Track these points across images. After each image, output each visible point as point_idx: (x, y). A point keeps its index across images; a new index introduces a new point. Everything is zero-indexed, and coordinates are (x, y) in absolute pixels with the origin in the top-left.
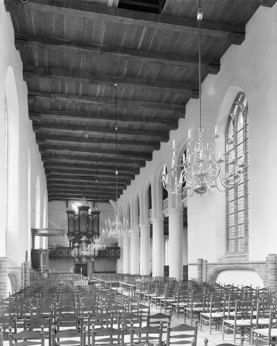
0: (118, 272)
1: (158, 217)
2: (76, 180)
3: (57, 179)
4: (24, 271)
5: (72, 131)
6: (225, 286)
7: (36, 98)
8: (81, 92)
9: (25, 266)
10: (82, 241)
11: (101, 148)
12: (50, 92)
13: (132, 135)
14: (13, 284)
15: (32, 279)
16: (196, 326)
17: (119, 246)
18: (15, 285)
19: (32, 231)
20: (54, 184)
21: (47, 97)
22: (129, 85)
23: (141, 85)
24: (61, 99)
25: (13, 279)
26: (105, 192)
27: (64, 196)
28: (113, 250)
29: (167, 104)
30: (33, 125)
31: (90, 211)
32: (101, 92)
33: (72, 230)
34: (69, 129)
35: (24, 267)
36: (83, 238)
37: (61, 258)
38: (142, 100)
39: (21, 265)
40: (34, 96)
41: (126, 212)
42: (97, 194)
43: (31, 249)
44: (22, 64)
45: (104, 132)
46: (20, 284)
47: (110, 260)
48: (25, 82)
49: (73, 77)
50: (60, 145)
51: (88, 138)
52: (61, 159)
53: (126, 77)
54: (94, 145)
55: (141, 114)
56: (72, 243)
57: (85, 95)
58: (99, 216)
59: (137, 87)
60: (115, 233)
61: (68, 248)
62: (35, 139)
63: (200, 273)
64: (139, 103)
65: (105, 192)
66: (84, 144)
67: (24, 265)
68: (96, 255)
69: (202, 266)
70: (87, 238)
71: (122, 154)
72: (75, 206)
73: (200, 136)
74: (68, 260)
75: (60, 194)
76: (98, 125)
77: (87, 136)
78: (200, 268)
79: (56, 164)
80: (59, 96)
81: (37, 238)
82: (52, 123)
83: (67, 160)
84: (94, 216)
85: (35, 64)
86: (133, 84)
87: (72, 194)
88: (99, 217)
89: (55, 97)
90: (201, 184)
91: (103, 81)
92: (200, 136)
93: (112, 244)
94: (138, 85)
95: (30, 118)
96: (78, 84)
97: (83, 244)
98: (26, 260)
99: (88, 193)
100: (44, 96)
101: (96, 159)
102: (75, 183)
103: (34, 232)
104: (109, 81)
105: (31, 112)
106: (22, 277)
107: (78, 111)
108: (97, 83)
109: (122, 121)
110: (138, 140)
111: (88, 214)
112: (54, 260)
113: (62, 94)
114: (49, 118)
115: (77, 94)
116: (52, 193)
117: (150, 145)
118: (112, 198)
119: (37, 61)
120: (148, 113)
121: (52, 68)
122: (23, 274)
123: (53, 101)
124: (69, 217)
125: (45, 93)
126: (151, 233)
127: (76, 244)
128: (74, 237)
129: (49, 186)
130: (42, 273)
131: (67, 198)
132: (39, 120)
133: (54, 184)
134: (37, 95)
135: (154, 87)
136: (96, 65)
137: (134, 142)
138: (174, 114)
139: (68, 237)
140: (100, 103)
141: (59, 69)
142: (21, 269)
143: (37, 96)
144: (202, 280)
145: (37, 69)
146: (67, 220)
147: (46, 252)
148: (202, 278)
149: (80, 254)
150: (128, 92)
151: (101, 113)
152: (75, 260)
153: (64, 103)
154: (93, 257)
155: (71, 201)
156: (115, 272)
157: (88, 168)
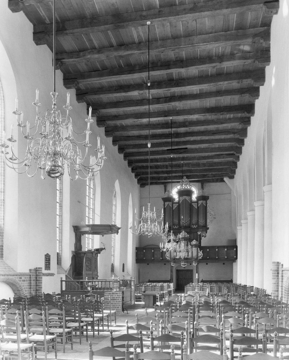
3: (138, 158)
5: (124, 93)
21: (76, 58)
22: (167, 18)
24: (92, 57)
26: (211, 168)
28: (226, 250)
29: (240, 31)
32: (139, 36)
34: (121, 92)
37: (153, 261)
39: (28, 271)
45: (166, 88)
47: (224, 264)
49: (92, 26)
50: (121, 113)
51: (153, 99)
53: (161, 9)
55: (209, 53)
57: (122, 45)
59: (178, 18)
60: (147, 228)
65: (211, 168)
68: (200, 258)
70: (186, 233)
73: (54, 102)
76: (156, 79)
80: (89, 53)
82: (99, 88)
84: (200, 202)
85: (46, 21)
86: (171, 16)
88: (206, 204)
91: (130, 21)
92: (54, 102)
93: (229, 241)
94: (178, 15)
100: (72, 58)
102: (165, 160)
107: (123, 67)
108: (123, 27)
109: (183, 68)
113: (93, 50)
114: (89, 82)
116: (142, 176)
117: (243, 93)
118: (226, 175)
119: (47, 18)
121: (66, 22)
125: (72, 54)
134: (63, 58)
135: (203, 13)
137: (219, 93)
140: (141, 51)
143: (64, 59)
147: (91, 254)
150: (175, 27)
156: (232, 281)
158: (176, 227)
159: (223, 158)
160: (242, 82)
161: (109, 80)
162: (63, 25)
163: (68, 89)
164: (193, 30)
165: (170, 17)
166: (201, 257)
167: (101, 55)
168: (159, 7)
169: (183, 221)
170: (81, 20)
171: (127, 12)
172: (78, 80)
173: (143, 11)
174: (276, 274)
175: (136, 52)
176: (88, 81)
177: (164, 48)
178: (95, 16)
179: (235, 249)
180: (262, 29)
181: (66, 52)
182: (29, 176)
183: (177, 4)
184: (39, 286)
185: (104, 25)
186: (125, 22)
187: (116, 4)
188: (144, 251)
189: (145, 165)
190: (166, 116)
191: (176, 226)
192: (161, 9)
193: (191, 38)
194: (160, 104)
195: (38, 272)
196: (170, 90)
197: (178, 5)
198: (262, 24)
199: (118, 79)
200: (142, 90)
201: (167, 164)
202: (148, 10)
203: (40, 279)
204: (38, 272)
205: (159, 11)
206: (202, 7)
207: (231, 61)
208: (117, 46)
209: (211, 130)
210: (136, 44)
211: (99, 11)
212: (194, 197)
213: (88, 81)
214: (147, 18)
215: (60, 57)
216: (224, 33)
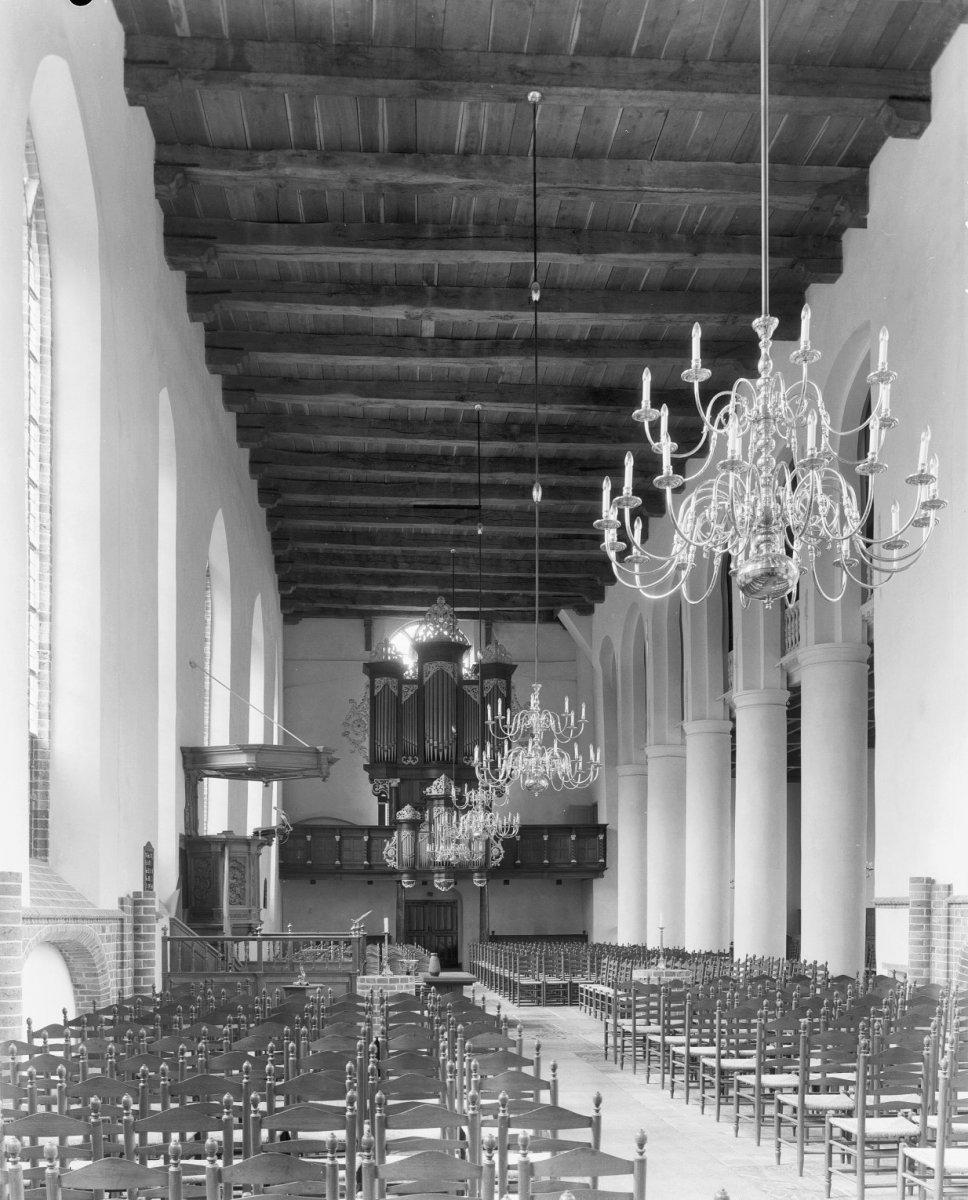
0: (597, 938)
1: (762, 687)
2: (403, 527)
4: (128, 932)
6: (32, 1035)
7: (190, 173)
8: (383, 135)
9: (136, 911)
10: (431, 799)
11: (497, 377)
12: (249, 145)
13: (628, 316)
14: (83, 987)
15: (180, 959)
16: (639, 1157)
17: (602, 819)
18: (90, 993)
19: (184, 758)
20: (306, 546)
21: (243, 170)
23: (647, 89)
25: (78, 965)
27: (354, 598)
28: (573, 837)
30: (188, 292)
31: (469, 661)
32: (473, 130)
33: (386, 750)
35: (131, 915)
36: (435, 782)
37: (338, 873)
38: (663, 157)
39: (115, 906)
40: (184, 165)
41: (631, 664)
42: (498, 582)
43: (181, 836)
44: (123, 34)
45: (501, 308)
46: (111, 988)
47: (559, 882)
48: (141, 112)
51: (437, 337)
52: (325, 434)
53: (580, 60)
54: (464, 366)
55: (665, 218)
56: (387, 805)
57: (405, 150)
58: (509, 683)
59: (631, 97)
61: (370, 829)
62: (200, 351)
63: (921, 943)
64: (649, 169)
66: (418, 364)
67: (129, 906)
68: (496, 862)
69: (929, 912)
71: (596, 403)
72: (404, 641)
74: (370, 883)
75: (333, 587)
76: (472, 277)
77: (428, 328)
78: (919, 920)
79: (306, 454)
80: (290, 159)
81: (215, 790)
83: (351, 440)
84: (490, 683)
85: (177, 27)
86: (611, 88)
87: (385, 588)
89: (274, 165)
90: (767, 556)
91: (478, 81)
93: (572, 809)
94: (634, 89)
95: (174, 264)
96: (367, 103)
97: (435, 809)
98: (149, 881)
99: (455, 580)
100: (227, 165)
101: (475, 426)
102: (398, 538)
103: (195, 763)
104: (503, 81)
105: (174, 235)
106: (122, 956)
107: (382, 220)
108: (448, 95)
110: (665, 333)
111: (460, 676)
112: (502, 881)
113: (305, 152)
115: (371, 148)
116: (301, 586)
120: (699, 212)
121: (250, 42)
122: (129, 943)
123: (267, 183)
124: (376, 692)
126: (794, 758)
127: (406, 813)
128: (398, 780)
129: (280, 552)
130: (229, 939)
131: (367, 607)
132: (214, 270)
133: (306, 546)
135: (708, 96)
136: (441, 15)
138: (817, 209)
139: (372, 780)
140: (471, 182)
141: (282, 45)
142: (116, 924)
144: (929, 973)
145: (184, 52)
146: (367, 704)
148: (928, 965)
149: (424, 857)
150: (598, 121)
151: (483, 222)
152: (400, 881)
153: (314, 192)
154: (479, 871)
155: (389, 620)
156: (584, 938)
157: (449, 471)
158: (410, 761)
159: (583, 548)
160: (733, 323)
161: (308, 258)
162: (230, 55)
163: (177, 269)
164: (646, 140)
165: (606, 91)
166: (500, 859)
167: (332, 172)
168: (575, 50)
169: (435, 742)
170: (304, 48)
171: (465, 49)
172: (217, 245)
173: (518, 53)
174: (925, 916)
175: (454, 180)
176: (252, 252)
177: (546, 182)
178: (358, 43)
179: (601, 837)
180: (847, 172)
181: (207, 145)
182: (835, 600)
183: (630, 54)
184: (145, 956)
185: (386, 78)
186: (459, 78)
187: (441, 15)
188: (309, 838)
189: (321, 551)
190: (462, 399)
191: (410, 758)
192: (580, 60)
193: (635, 164)
194: (459, 357)
195: (145, 909)
196: (512, 317)
197: (634, 57)
198: (847, 157)
199: (343, 259)
200: (422, 305)
201: (395, 553)
202: (537, 54)
203: (149, 931)
204: (145, 909)
205: (573, 65)
206: (706, 75)
207: (728, 253)
208: (390, 151)
209: (578, 456)
210: (453, 153)
211: (376, 31)
212: (469, 661)
213: (252, 252)
214: (534, 80)
215: (178, 154)
216: (734, 164)
